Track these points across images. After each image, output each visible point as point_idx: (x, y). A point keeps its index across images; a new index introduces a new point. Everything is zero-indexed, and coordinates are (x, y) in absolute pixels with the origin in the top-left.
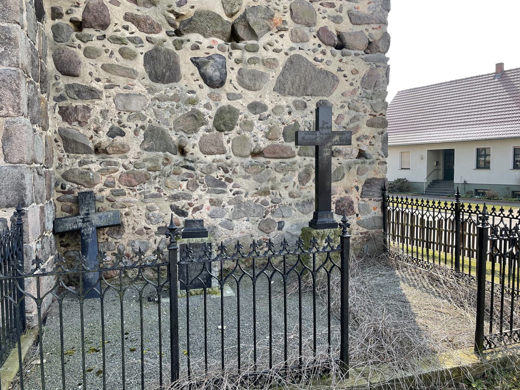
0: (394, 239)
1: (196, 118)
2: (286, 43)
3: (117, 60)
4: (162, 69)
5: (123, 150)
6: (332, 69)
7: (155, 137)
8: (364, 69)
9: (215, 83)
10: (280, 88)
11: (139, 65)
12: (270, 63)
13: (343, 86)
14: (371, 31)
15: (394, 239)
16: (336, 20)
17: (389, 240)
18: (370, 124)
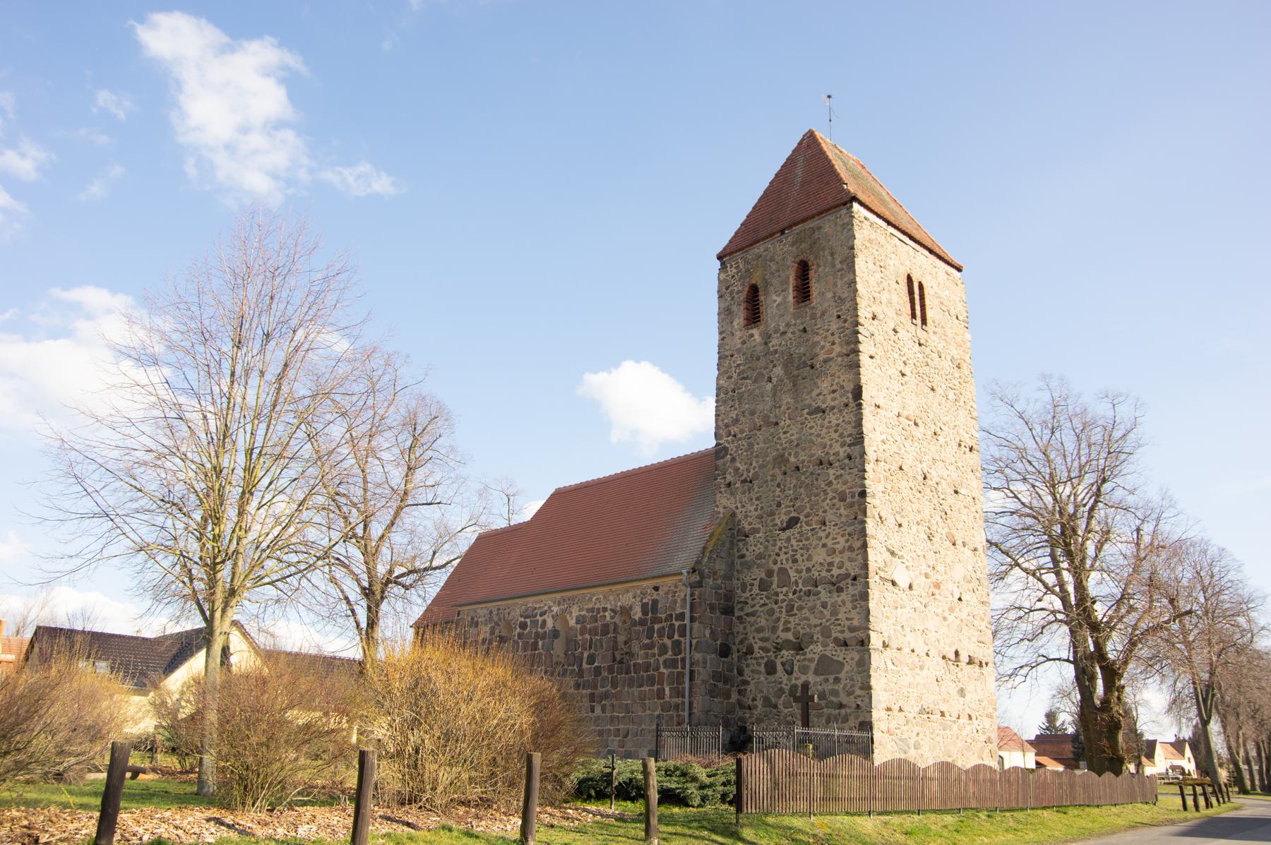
0: (793, 244)
1: (781, 691)
2: (820, 648)
3: (756, 667)
4: (771, 669)
5: (756, 707)
6: (840, 659)
7: (767, 701)
8: (857, 656)
9: (790, 673)
10: (816, 672)
11: (762, 669)
12: (811, 660)
13: (847, 668)
14: (860, 635)
15: (793, 244)
16: (842, 632)
17: (230, 541)
18: (861, 689)
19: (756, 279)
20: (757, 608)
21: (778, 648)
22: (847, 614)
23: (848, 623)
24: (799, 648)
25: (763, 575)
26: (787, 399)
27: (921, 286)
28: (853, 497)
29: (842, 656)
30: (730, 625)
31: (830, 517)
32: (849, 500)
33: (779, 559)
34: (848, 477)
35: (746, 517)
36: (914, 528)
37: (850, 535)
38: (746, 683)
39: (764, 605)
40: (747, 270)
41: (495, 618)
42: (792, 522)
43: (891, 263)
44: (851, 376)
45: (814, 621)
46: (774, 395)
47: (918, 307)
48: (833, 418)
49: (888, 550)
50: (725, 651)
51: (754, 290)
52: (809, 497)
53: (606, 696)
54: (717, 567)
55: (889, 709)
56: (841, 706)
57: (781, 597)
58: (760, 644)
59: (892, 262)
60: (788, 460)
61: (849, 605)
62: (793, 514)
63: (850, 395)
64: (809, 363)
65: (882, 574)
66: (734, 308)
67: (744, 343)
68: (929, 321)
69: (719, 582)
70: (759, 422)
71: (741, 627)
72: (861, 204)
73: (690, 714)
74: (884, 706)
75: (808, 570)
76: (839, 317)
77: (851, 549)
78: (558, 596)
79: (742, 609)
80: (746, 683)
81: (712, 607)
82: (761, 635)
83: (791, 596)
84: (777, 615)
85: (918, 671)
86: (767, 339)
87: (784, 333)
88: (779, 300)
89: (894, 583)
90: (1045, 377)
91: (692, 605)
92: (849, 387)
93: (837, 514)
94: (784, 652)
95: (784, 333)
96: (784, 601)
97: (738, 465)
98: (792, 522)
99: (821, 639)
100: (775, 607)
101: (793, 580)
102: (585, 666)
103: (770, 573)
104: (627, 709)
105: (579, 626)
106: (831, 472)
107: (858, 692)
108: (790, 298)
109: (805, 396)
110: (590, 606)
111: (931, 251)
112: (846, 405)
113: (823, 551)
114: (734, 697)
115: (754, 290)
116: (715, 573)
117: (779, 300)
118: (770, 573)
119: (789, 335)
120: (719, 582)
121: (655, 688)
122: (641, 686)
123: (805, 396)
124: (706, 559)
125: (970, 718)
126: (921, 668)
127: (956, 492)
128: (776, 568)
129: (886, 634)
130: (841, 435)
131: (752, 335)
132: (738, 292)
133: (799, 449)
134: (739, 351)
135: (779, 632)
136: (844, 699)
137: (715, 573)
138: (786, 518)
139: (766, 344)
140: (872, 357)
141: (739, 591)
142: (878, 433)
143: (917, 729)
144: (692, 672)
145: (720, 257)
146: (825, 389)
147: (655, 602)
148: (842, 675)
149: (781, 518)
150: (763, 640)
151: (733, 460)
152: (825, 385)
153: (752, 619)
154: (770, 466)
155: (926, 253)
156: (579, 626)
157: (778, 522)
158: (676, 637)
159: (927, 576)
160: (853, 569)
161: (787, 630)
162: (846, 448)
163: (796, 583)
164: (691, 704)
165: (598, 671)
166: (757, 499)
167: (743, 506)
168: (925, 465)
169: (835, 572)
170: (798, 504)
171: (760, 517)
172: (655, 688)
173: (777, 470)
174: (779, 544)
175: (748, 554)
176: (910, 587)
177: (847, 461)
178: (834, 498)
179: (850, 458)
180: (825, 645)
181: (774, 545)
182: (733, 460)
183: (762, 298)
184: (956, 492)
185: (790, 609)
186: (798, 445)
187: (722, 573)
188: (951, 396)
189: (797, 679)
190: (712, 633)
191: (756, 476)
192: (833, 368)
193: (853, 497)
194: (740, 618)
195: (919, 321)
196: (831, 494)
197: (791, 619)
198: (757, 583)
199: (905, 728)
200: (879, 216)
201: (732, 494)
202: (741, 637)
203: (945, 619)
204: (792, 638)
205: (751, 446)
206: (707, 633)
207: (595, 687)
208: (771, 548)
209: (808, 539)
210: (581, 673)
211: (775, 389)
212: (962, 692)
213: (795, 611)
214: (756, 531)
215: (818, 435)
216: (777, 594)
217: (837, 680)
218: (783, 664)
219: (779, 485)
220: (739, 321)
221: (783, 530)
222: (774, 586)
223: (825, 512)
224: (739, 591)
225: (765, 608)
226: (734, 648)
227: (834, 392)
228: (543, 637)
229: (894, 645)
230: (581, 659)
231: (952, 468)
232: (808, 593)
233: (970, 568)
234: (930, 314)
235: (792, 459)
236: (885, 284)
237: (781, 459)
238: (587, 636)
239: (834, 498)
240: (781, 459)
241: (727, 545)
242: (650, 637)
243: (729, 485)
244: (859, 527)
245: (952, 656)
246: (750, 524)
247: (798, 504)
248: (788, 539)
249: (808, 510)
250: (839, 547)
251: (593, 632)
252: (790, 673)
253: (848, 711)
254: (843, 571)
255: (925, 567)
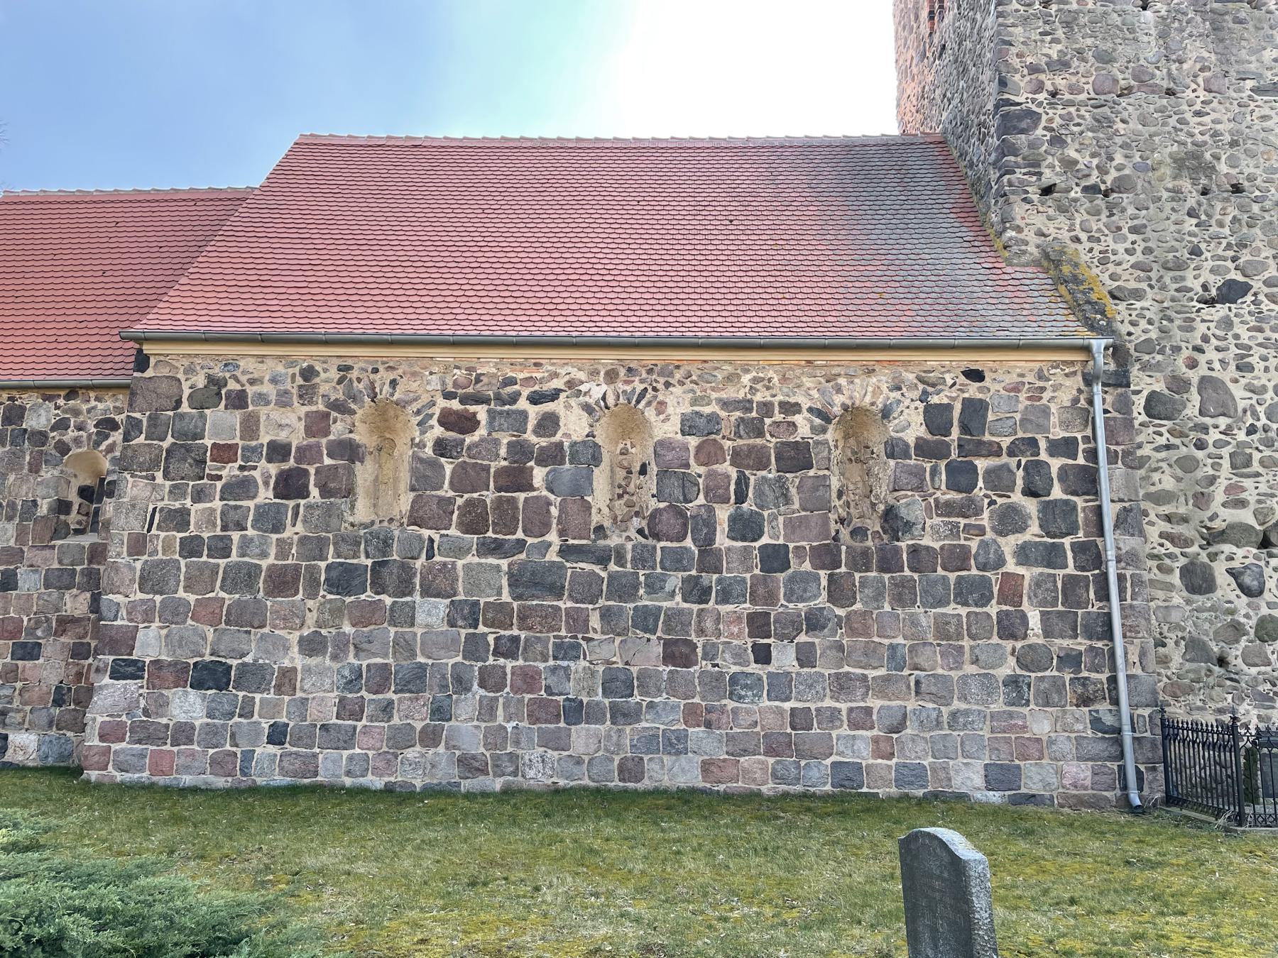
1: (1237, 629)
7: (1195, 648)
11: (1176, 578)
21: (1213, 538)
26: (1196, 51)
33: (1202, 359)
35: (1103, 262)
46: (1163, 35)
78: (607, 358)
82: (1167, 509)
83: (1241, 436)
96: (1218, 444)
98: (1231, 292)
102: (722, 541)
104: (895, 658)
105: (693, 442)
110: (731, 393)
118: (1179, 385)
121: (993, 609)
122: (942, 602)
128: (1194, 376)
133: (1238, 152)
135: (1216, 506)
138: (1215, 282)
147: (975, 410)
151: (1058, 141)
156: (693, 442)
165: (775, 559)
170: (1245, 256)
172: (993, 609)
173: (1186, 184)
174: (1201, 328)
182: (1058, 141)
186: (1234, 144)
197: (1248, 483)
201: (1062, 210)
204: (1252, 521)
210: (709, 559)
219: (1191, 213)
221: (1211, 302)
225: (1173, 455)
228: (552, 456)
230: (711, 524)
235: (1223, 168)
243: (1047, 191)
246: (1113, 277)
247: (1245, 256)
248: (1227, 323)
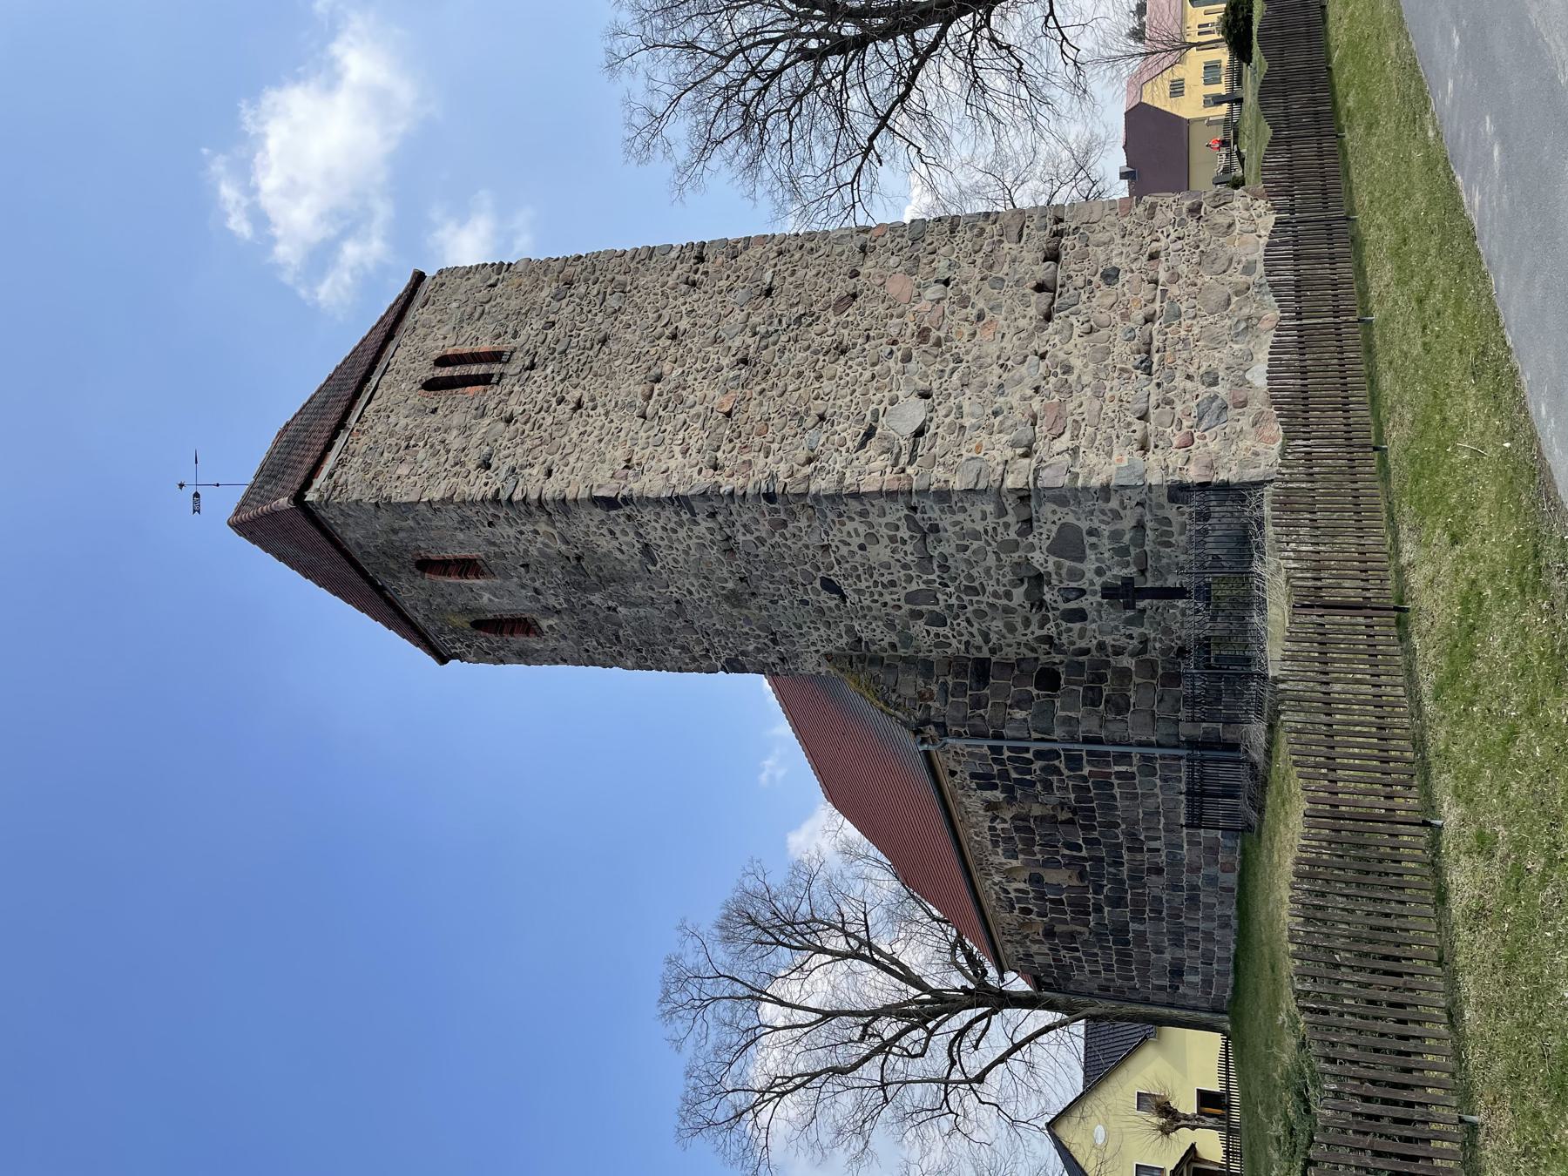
3: (1075, 634)
6: (1055, 528)
9: (1082, 592)
10: (1081, 558)
12: (1059, 566)
13: (1071, 519)
14: (1010, 503)
19: (462, 621)
20: (974, 630)
22: (978, 515)
23: (990, 519)
24: (1039, 579)
25: (921, 622)
26: (638, 590)
27: (442, 361)
28: (777, 511)
29: (1049, 525)
30: (1006, 666)
31: (814, 540)
32: (783, 516)
34: (745, 517)
36: (827, 385)
37: (840, 515)
38: (1101, 646)
39: (968, 621)
40: (453, 631)
41: (1018, 938)
42: (829, 585)
43: (403, 422)
44: (583, 513)
45: (991, 560)
47: (475, 369)
48: (655, 535)
49: (862, 445)
50: (1048, 679)
51: (478, 625)
52: (785, 566)
53: (1132, 836)
54: (911, 692)
55: (1144, 448)
56: (1140, 526)
57: (953, 601)
58: (1034, 627)
59: (401, 420)
60: (733, 591)
61: (960, 517)
62: (817, 584)
63: (613, 513)
64: (574, 562)
65: (904, 459)
66: (515, 646)
67: (564, 637)
68: (497, 346)
69: (935, 688)
70: (679, 623)
71: (1006, 649)
72: (307, 484)
73: (1159, 745)
74: (1137, 455)
75: (905, 567)
76: (490, 524)
77: (863, 514)
79: (979, 649)
80: (1101, 646)
81: (978, 703)
84: (983, 606)
85: (1072, 378)
86: (548, 611)
87: (536, 591)
88: (486, 596)
89: (920, 433)
90: (614, 64)
91: (975, 735)
92: (599, 514)
93: (805, 533)
94: (1047, 597)
95: (536, 591)
96: (958, 597)
97: (751, 648)
98: (829, 585)
99: (1021, 553)
100: (970, 608)
101: (923, 586)
103: (918, 615)
105: (1021, 856)
106: (740, 538)
107: (1114, 504)
108: (481, 582)
109: (628, 568)
111: (389, 336)
112: (629, 517)
113: (872, 550)
114: (1127, 662)
115: (478, 625)
116: (921, 696)
117: (488, 596)
119: (537, 584)
120: (935, 688)
121: (1116, 782)
122: (1114, 797)
123: (628, 568)
124: (899, 714)
125: (1153, 256)
126: (1068, 370)
127: (769, 292)
128: (906, 607)
129: (1009, 453)
130: (681, 525)
131: (550, 627)
132: (488, 640)
134: (578, 643)
135: (1014, 604)
136: (1128, 523)
137: (921, 696)
138: (824, 595)
139: (558, 612)
140: (549, 473)
141: (949, 651)
142: (672, 464)
143: (1180, 382)
144: (1087, 741)
145: (443, 660)
146: (613, 543)
148: (1084, 525)
149: (828, 600)
150: (1027, 623)
152: (605, 544)
153: (994, 637)
154: (745, 612)
155: (391, 347)
156: (1021, 856)
157: (832, 604)
158: (1030, 756)
159: (907, 358)
160: (897, 512)
161: (1008, 595)
162: (699, 518)
163: (927, 582)
164: (1140, 744)
166: (800, 627)
167: (814, 644)
168: (725, 362)
169: (904, 533)
171: (828, 625)
172: (1116, 782)
174: (866, 603)
175: (887, 640)
176: (925, 395)
177: (720, 518)
178: (783, 535)
179: (713, 515)
180: (1032, 547)
181: (870, 609)
183: (490, 616)
184: (769, 292)
185: (973, 591)
187: (920, 681)
188: (613, 302)
189: (1092, 583)
190: (1019, 704)
191: (767, 629)
192: (576, 532)
193: (777, 511)
194: (993, 651)
195: (496, 368)
196: (777, 538)
197: (990, 589)
198: (933, 630)
199: (1179, 407)
200: (329, 447)
202: (1023, 650)
203: (980, 317)
205: (718, 633)
206: (1019, 714)
207: (1120, 846)
208: (874, 613)
209: (855, 568)
211: (627, 604)
212: (1111, 276)
213: (976, 584)
214: (850, 629)
215: (686, 553)
216: (950, 607)
217: (1091, 532)
218: (1067, 600)
220: (533, 642)
221: (843, 598)
222: (936, 608)
223: (807, 547)
224: (949, 651)
226: (1043, 658)
227: (612, 532)
229: (1025, 433)
231: (730, 298)
232: (944, 568)
233: (893, 261)
234: (485, 346)
235: (730, 585)
236: (436, 438)
237: (734, 598)
238: (1036, 849)
239: (783, 535)
240: (734, 598)
241: (875, 670)
242: (1032, 784)
243: (783, 660)
244: (825, 504)
245: (1045, 297)
248: (859, 592)
249: (807, 567)
250: (862, 529)
251: (1029, 843)
252: (1082, 592)
253: (1148, 517)
254: (903, 524)
255: (891, 363)
